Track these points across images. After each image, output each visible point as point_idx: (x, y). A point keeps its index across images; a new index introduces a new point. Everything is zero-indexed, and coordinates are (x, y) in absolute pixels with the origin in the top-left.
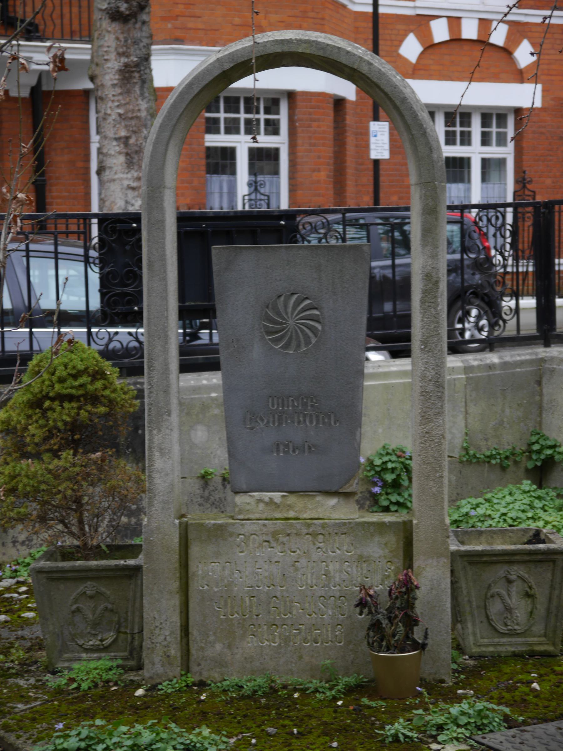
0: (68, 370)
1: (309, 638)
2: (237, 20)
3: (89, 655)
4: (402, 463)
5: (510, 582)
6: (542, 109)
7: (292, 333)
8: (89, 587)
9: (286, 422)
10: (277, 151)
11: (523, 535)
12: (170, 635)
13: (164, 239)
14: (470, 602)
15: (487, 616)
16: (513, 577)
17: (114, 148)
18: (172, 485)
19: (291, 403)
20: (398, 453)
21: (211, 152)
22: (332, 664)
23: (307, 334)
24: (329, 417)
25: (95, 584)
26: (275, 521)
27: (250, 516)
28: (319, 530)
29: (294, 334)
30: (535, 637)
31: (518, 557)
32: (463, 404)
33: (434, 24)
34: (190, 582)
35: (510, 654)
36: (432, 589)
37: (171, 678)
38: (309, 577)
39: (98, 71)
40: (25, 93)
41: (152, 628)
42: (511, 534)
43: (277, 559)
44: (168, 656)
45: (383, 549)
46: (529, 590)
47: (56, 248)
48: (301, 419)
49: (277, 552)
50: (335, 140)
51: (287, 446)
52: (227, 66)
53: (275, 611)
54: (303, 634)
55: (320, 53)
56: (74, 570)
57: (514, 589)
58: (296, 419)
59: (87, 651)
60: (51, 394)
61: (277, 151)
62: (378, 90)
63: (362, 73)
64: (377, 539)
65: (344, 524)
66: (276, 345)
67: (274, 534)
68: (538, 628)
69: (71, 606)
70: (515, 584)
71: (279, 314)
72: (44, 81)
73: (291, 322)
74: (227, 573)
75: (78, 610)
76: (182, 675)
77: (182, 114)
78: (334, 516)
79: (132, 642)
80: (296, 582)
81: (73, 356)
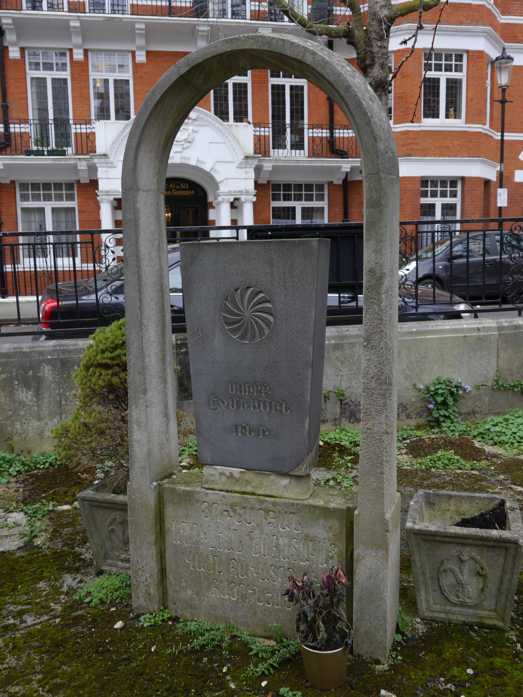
1: (262, 598)
2: (437, 145)
3: (123, 564)
4: (450, 390)
5: (462, 561)
7: (248, 324)
9: (243, 406)
10: (456, 204)
11: (489, 503)
12: (150, 577)
14: (423, 573)
15: (440, 587)
16: (465, 558)
19: (247, 389)
20: (447, 384)
21: (423, 206)
23: (261, 326)
25: (122, 514)
26: (233, 494)
27: (214, 487)
29: (249, 326)
30: (485, 610)
31: (470, 541)
32: (496, 351)
35: (460, 623)
36: (370, 577)
38: (262, 547)
40: (340, 182)
41: (136, 569)
42: (478, 501)
44: (149, 594)
45: (327, 532)
46: (480, 571)
49: (235, 522)
50: (484, 199)
51: (244, 428)
53: (233, 571)
54: (257, 594)
55: (266, 48)
56: (105, 502)
57: (466, 568)
61: (456, 204)
63: (307, 64)
64: (322, 522)
65: (293, 504)
67: (233, 505)
68: (489, 603)
70: (467, 563)
71: (236, 307)
72: (349, 176)
73: (247, 314)
74: (195, 532)
76: (161, 610)
78: (286, 495)
80: (251, 549)
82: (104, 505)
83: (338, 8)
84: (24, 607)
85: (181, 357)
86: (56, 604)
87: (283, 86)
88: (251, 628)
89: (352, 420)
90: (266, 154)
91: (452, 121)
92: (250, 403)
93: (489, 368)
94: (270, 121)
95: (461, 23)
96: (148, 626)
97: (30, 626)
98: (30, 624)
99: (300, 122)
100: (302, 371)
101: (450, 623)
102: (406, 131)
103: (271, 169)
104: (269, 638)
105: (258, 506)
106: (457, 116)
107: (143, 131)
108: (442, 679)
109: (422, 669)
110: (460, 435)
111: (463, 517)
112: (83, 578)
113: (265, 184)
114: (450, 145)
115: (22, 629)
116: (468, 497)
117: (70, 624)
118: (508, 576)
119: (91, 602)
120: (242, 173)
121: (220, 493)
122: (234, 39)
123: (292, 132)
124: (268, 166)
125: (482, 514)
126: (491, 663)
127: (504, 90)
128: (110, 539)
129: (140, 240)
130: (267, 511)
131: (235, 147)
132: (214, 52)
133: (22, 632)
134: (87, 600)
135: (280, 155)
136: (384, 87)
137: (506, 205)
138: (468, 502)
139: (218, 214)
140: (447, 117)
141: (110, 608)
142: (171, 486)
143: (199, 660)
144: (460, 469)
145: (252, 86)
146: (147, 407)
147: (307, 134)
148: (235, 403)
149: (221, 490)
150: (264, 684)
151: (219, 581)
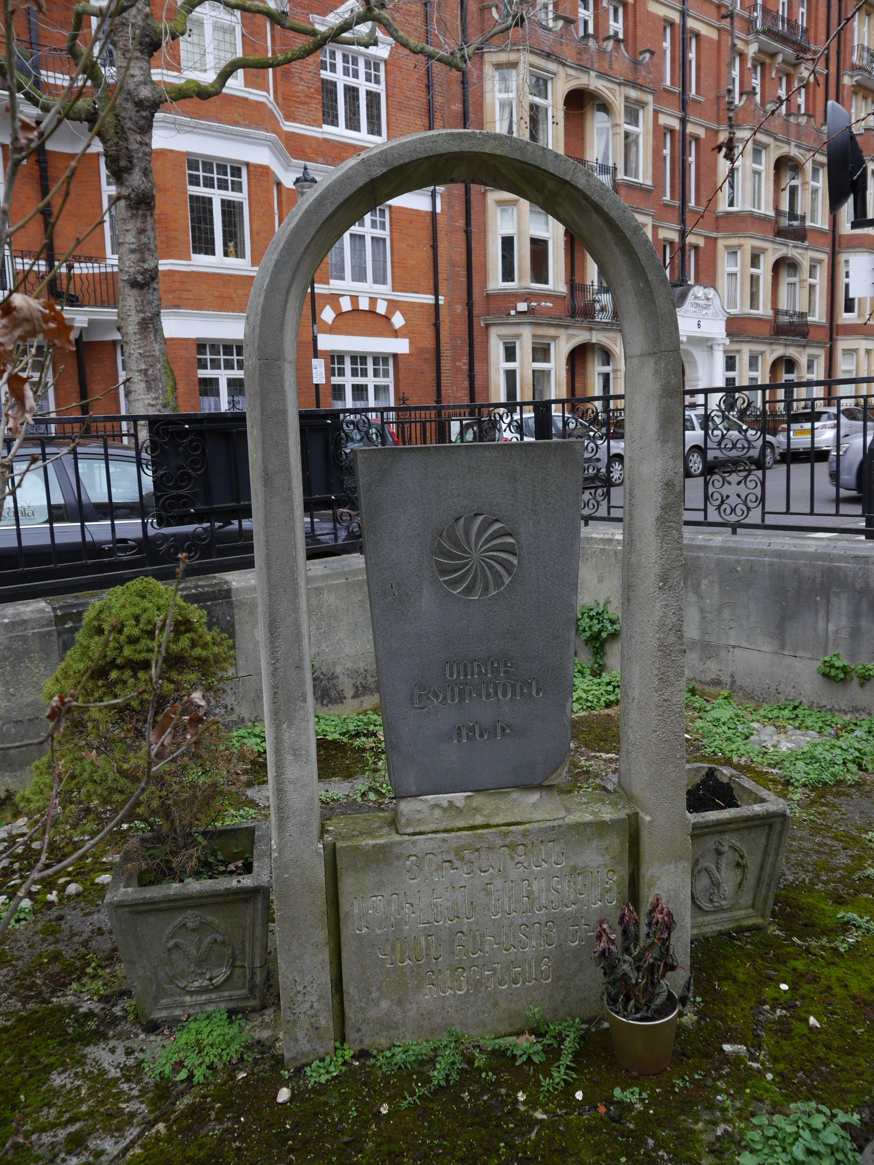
0: (141, 626)
1: (506, 978)
2: (216, 294)
5: (719, 853)
8: (190, 918)
9: (470, 696)
12: (318, 1000)
13: (287, 439)
17: (137, 377)
19: (476, 670)
23: (497, 571)
26: (459, 833)
27: (422, 828)
28: (520, 839)
33: (341, 299)
34: (343, 926)
37: (322, 1055)
39: (123, 324)
41: (292, 994)
44: (317, 1028)
45: (603, 856)
47: (106, 451)
49: (462, 875)
52: (378, 171)
54: (498, 974)
55: (517, 156)
56: (167, 900)
57: (723, 862)
58: (484, 692)
59: (191, 993)
60: (118, 661)
62: (595, 217)
64: (595, 843)
65: (553, 828)
66: (455, 590)
67: (458, 851)
68: (746, 899)
71: (457, 544)
72: (84, 335)
73: (475, 555)
74: (393, 908)
75: (176, 946)
76: (336, 1048)
77: (308, 245)
78: (536, 816)
79: (252, 978)
81: (146, 604)
82: (163, 905)
84: (72, 1129)
85: (65, 636)
88: (489, 1028)
89: (325, 702)
91: (232, 261)
95: (236, 123)
96: (327, 1081)
98: (116, 1153)
101: (707, 939)
102: (170, 271)
103: (86, 325)
104: (518, 1033)
105: (500, 842)
106: (239, 253)
107: (299, 263)
108: (767, 1007)
114: (234, 295)
117: (193, 1124)
118: (771, 859)
119: (191, 1076)
121: (438, 836)
126: (795, 969)
130: (512, 847)
132: (431, 149)
134: (183, 1075)
136: (149, 204)
140: (226, 254)
141: (233, 1077)
142: (349, 843)
143: (458, 1100)
148: (456, 694)
150: (579, 1095)
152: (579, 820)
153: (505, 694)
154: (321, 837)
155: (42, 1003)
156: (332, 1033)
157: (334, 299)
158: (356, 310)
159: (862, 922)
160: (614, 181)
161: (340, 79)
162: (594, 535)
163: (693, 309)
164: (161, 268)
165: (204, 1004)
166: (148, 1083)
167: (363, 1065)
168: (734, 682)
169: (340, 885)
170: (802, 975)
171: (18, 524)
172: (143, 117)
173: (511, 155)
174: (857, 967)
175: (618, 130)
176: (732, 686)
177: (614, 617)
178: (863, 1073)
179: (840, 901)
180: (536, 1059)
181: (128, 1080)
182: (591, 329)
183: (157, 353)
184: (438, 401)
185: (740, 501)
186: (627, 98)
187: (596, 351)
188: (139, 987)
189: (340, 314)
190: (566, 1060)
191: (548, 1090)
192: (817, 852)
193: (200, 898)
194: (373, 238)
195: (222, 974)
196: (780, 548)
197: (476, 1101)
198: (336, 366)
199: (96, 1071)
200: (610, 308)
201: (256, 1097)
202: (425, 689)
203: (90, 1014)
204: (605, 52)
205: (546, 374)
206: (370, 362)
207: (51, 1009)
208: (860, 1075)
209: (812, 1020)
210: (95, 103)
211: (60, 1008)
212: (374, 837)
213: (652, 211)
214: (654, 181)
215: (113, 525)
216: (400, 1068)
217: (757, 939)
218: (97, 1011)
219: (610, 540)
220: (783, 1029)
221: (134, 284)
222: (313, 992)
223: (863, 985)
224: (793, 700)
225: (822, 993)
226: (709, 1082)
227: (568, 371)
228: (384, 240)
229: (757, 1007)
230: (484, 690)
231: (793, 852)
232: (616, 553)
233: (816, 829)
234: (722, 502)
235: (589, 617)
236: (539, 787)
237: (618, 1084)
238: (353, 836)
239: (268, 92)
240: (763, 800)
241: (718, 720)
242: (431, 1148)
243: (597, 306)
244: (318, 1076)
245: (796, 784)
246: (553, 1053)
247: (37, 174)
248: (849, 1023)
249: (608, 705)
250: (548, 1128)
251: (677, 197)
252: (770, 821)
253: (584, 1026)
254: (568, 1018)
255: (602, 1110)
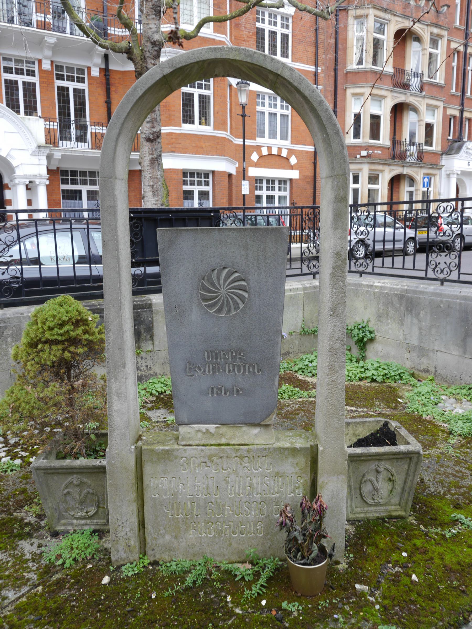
1: (237, 531)
2: (194, 145)
3: (78, 521)
5: (378, 472)
6: (299, 179)
7: (224, 300)
8: (75, 479)
9: (219, 370)
10: (208, 192)
12: (130, 531)
13: (116, 222)
15: (361, 494)
18: (128, 422)
19: (223, 356)
22: (254, 552)
23: (236, 301)
24: (254, 367)
25: (79, 476)
26: (211, 447)
27: (191, 443)
30: (392, 505)
31: (386, 457)
33: (262, 149)
34: (145, 492)
38: (237, 488)
39: (142, 161)
41: (116, 526)
42: (368, 424)
43: (212, 475)
44: (129, 546)
45: (295, 467)
46: (391, 477)
47: (88, 226)
48: (231, 368)
49: (212, 471)
53: (211, 513)
54: (232, 528)
55: (249, 60)
56: (62, 468)
57: (381, 477)
59: (77, 519)
61: (208, 192)
64: (290, 460)
66: (211, 310)
67: (210, 457)
68: (395, 500)
69: (64, 490)
71: (213, 284)
73: (223, 291)
75: (68, 493)
76: (140, 558)
78: (257, 442)
80: (227, 491)
82: (60, 471)
83: (113, 29)
86: (29, 572)
87: (68, 88)
88: (226, 557)
90: (55, 144)
92: (225, 367)
93: (298, 319)
94: (57, 117)
96: (132, 575)
97: (13, 601)
98: (13, 599)
99: (83, 119)
100: (273, 337)
101: (369, 520)
102: (170, 133)
103: (60, 158)
104: (243, 562)
106: (207, 124)
107: (123, 124)
108: (390, 565)
109: (372, 561)
110: (284, 372)
111: (358, 437)
112: (41, 541)
113: (55, 170)
114: (204, 146)
115: (7, 606)
116: (361, 422)
117: (56, 589)
118: (410, 478)
119: (64, 563)
120: (35, 160)
121: (199, 448)
122: (218, 48)
123: (77, 128)
124: (57, 155)
125: (372, 434)
126: (414, 545)
127: (244, 107)
128: (66, 502)
129: (118, 226)
130: (241, 458)
131: (28, 137)
133: (9, 608)
134: (60, 562)
135: (68, 146)
137: (248, 193)
138: (361, 426)
139: (15, 194)
141: (85, 566)
142: (149, 447)
143: (196, 595)
144: (300, 397)
145: (40, 86)
146: (126, 379)
147: (90, 130)
148: (211, 369)
149: (197, 445)
150: (264, 603)
151: (197, 523)
152: (282, 446)
153: (239, 371)
154: (136, 442)
155: (8, 515)
156: (137, 549)
157: (258, 148)
158: (270, 155)
159: (466, 521)
160: (421, 81)
161: (267, 27)
162: (364, 283)
163: (466, 155)
164: (162, 131)
165: (83, 525)
166: (42, 564)
167: (154, 569)
168: (436, 371)
169: (143, 469)
170: (418, 549)
171: (57, 265)
172: (155, 50)
173: (245, 60)
174: (453, 548)
175: (425, 52)
176: (435, 373)
177: (371, 330)
178: (435, 613)
179: (457, 507)
180: (246, 578)
181: (33, 561)
182: (403, 166)
183: (159, 176)
184: (244, 205)
185: (445, 266)
186: (431, 33)
187: (406, 179)
188: (49, 512)
189: (261, 157)
190: (262, 581)
191: (247, 597)
192: (454, 476)
193: (80, 469)
194: (281, 115)
195: (93, 510)
196: (466, 294)
197: (207, 597)
198: (258, 185)
199: (20, 554)
200: (416, 154)
201: (92, 579)
202: (193, 365)
203: (29, 524)
204: (420, 7)
205: (376, 191)
206: (277, 183)
207: (12, 519)
208: (433, 613)
209: (414, 577)
210: (129, 43)
211: (16, 519)
212: (164, 445)
213: (443, 99)
214: (445, 81)
215: (90, 267)
216: (172, 573)
217: (399, 524)
218: (32, 522)
219: (372, 286)
220: (395, 580)
221: (148, 140)
222: (127, 526)
223: (453, 559)
224: (469, 384)
225: (427, 561)
226: (340, 605)
227: (388, 190)
228: (288, 116)
229: (385, 565)
230: (227, 368)
231: (440, 474)
232: (374, 293)
233: (458, 462)
234: (436, 266)
235: (358, 328)
236: (259, 425)
237: (287, 599)
238: (154, 443)
239: (226, 35)
240: (408, 443)
241: (420, 393)
242: (172, 621)
243: (408, 153)
244: (127, 571)
245: (455, 434)
246: (257, 575)
247: (104, 82)
248: (436, 581)
249: (361, 379)
250: (239, 619)
251: (459, 90)
252: (410, 456)
253: (280, 563)
254: (272, 557)
255: (274, 613)
